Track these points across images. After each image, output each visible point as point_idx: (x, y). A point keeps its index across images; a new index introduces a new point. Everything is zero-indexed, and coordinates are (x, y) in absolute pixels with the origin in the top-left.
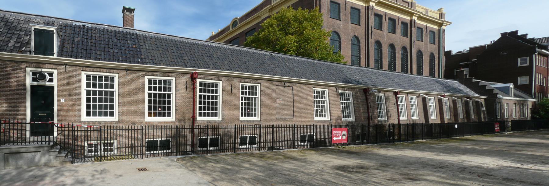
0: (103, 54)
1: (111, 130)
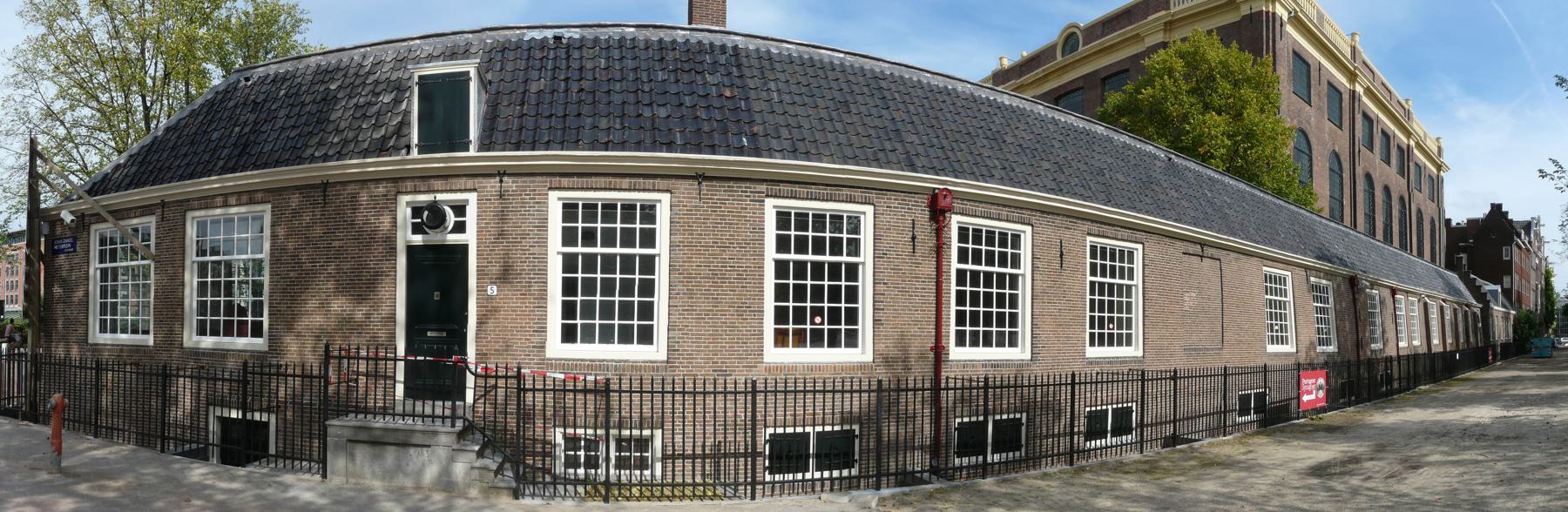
0: (618, 126)
1: (641, 392)
